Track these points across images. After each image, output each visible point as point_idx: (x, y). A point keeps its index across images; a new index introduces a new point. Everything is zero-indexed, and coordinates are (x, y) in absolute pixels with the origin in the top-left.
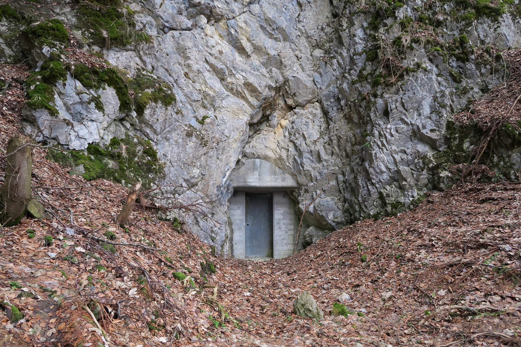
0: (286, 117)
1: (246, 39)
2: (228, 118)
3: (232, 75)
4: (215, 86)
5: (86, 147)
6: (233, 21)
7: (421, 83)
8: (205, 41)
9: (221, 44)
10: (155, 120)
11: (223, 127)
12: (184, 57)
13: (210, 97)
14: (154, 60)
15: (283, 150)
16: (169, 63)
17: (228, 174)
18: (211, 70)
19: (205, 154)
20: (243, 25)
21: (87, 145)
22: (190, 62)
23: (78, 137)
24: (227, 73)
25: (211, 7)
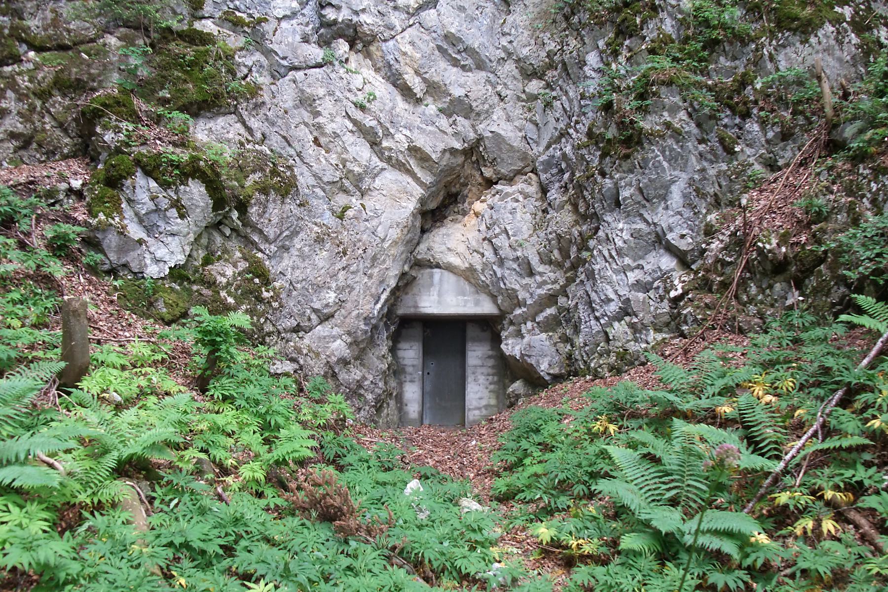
0: (483, 198)
1: (413, 72)
2: (383, 207)
3: (388, 134)
4: (361, 157)
5: (167, 273)
6: (391, 43)
7: (670, 155)
8: (345, 81)
9: (373, 83)
10: (267, 221)
11: (375, 222)
12: (311, 112)
13: (354, 175)
14: (266, 124)
15: (475, 254)
16: (288, 127)
17: (384, 297)
18: (354, 129)
19: (344, 269)
20: (408, 49)
21: (168, 270)
22: (320, 120)
23: (157, 261)
24: (380, 134)
25: (355, 25)
